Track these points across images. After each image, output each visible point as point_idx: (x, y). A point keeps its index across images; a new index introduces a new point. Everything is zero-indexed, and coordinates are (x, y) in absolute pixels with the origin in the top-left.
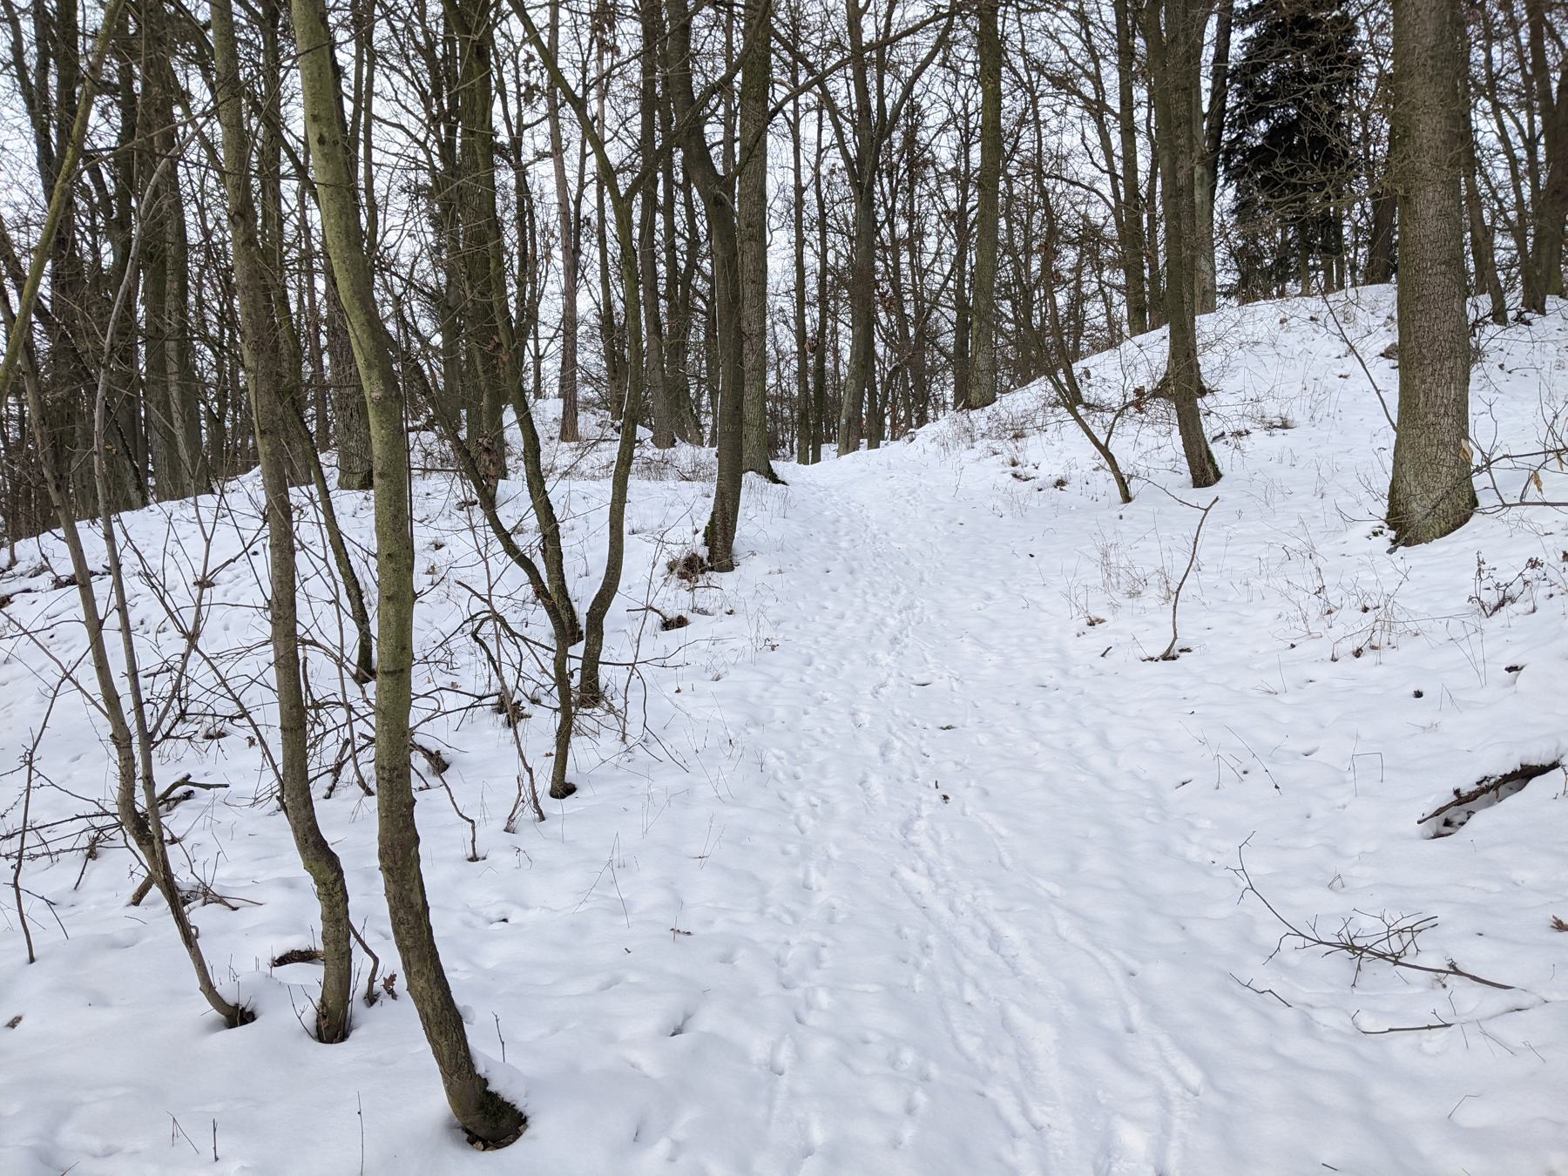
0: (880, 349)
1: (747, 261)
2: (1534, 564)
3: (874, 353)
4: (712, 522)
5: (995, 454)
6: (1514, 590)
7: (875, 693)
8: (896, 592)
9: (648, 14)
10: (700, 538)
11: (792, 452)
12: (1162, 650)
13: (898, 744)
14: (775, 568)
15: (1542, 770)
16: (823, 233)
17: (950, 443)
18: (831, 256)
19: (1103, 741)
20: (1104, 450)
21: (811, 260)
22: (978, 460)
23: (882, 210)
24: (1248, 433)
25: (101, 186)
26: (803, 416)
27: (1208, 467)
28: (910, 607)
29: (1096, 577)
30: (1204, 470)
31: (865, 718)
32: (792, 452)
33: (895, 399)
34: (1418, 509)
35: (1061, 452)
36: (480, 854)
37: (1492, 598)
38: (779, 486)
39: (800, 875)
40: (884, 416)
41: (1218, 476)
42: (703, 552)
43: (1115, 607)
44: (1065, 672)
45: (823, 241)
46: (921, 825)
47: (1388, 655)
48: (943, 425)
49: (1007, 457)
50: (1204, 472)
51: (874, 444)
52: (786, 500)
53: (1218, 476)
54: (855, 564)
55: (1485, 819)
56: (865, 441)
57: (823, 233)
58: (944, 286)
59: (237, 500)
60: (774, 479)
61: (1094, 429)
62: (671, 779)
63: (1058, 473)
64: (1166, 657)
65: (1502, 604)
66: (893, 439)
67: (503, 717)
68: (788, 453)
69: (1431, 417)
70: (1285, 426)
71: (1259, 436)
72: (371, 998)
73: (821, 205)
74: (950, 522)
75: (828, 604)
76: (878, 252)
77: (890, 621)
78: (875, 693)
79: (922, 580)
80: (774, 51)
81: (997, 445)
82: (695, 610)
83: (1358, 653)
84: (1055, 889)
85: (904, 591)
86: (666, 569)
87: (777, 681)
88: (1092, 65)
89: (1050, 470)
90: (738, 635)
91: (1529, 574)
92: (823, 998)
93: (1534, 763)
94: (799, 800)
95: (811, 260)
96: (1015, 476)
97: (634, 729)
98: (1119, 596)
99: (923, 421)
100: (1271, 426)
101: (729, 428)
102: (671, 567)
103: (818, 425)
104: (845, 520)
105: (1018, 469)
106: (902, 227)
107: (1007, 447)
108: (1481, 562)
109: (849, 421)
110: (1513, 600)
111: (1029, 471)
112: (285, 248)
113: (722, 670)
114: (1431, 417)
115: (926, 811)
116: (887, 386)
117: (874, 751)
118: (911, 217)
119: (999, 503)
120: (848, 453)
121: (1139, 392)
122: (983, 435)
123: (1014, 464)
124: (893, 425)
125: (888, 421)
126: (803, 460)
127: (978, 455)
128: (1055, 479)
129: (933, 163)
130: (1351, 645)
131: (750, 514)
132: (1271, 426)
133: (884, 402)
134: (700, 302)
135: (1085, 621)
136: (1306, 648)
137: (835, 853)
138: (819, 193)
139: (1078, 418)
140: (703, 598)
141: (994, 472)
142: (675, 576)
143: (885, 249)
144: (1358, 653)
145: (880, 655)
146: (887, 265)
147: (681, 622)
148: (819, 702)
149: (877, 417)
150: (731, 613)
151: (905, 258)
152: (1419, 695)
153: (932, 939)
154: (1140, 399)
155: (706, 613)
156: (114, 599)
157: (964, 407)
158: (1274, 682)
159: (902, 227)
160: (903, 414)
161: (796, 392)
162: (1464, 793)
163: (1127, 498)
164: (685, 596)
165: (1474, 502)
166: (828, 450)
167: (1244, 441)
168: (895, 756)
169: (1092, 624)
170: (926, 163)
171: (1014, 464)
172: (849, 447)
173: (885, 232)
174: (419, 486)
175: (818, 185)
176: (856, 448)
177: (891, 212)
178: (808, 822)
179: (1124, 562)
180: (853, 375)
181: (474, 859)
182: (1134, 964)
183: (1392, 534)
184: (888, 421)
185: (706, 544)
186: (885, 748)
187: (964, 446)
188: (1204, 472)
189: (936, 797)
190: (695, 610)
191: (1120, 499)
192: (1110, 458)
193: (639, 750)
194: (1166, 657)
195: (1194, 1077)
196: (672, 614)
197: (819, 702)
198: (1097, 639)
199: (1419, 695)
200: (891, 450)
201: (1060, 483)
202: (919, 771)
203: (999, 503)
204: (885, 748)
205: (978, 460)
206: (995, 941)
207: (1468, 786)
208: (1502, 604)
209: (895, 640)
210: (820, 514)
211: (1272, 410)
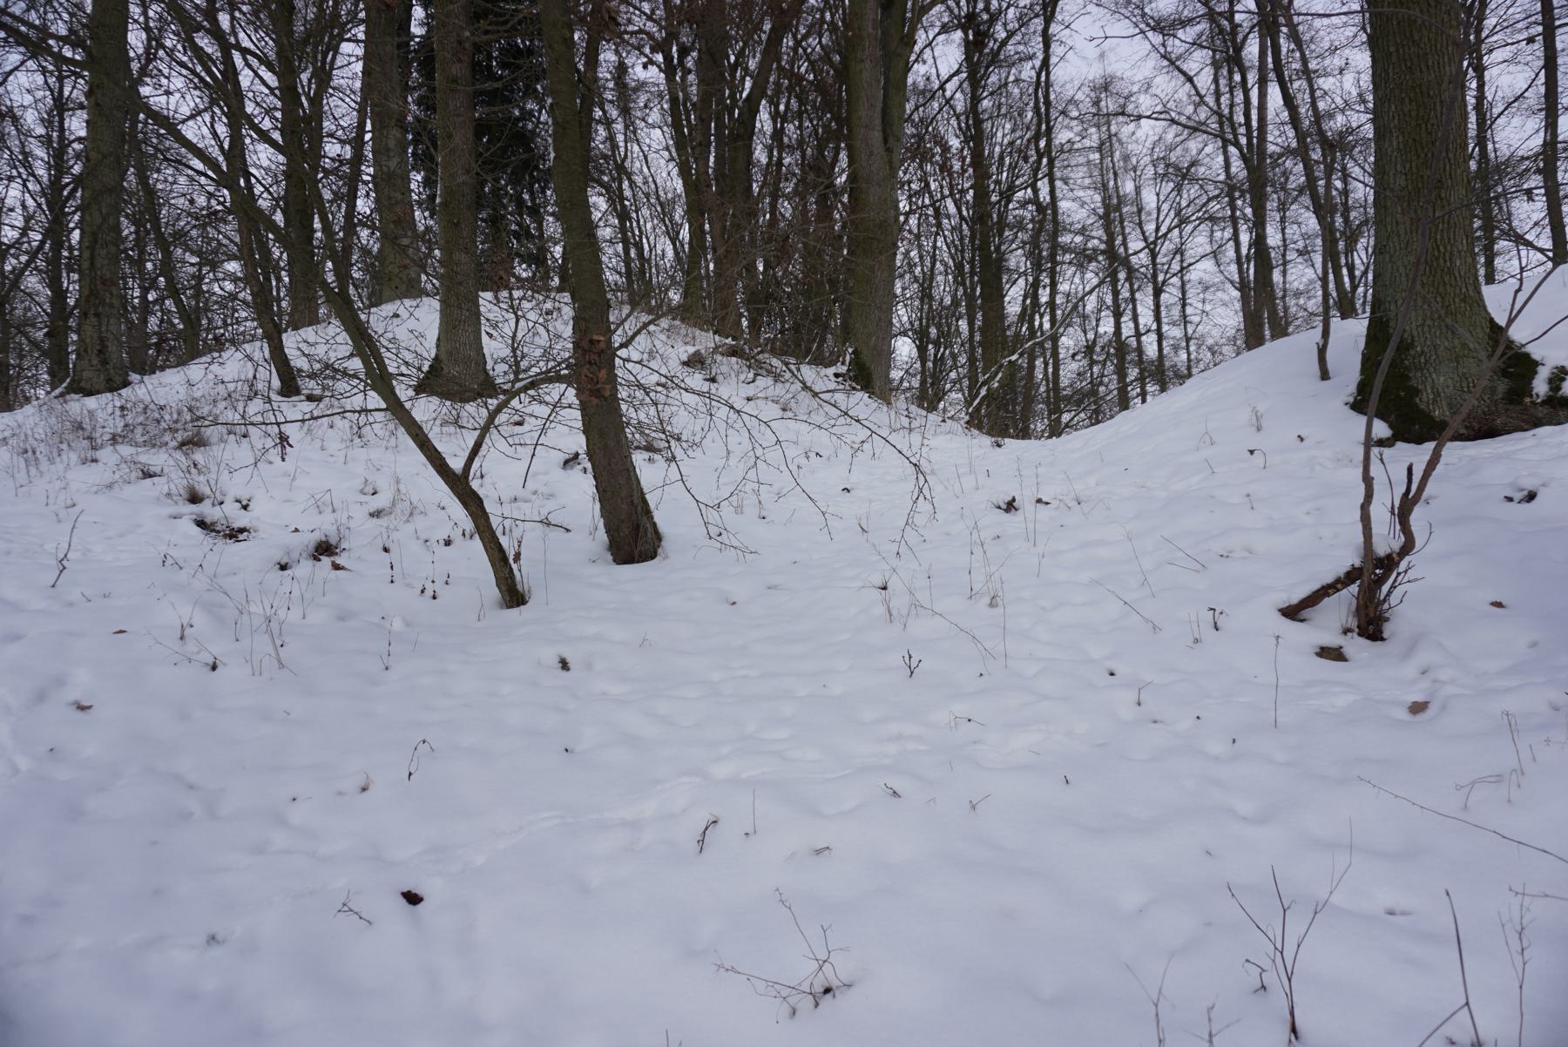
5: (147, 475)
9: (1480, 2)
17: (42, 448)
22: (110, 486)
25: (211, 179)
49: (177, 482)
59: (140, 45)
74: (40, 697)
80: (550, 136)
81: (155, 459)
96: (201, 524)
105: (207, 510)
112: (902, 218)
122: (114, 439)
127: (108, 477)
156: (1213, 87)
157: (70, 390)
171: (195, 498)
187: (74, 457)
191: (493, 592)
205: (110, 486)
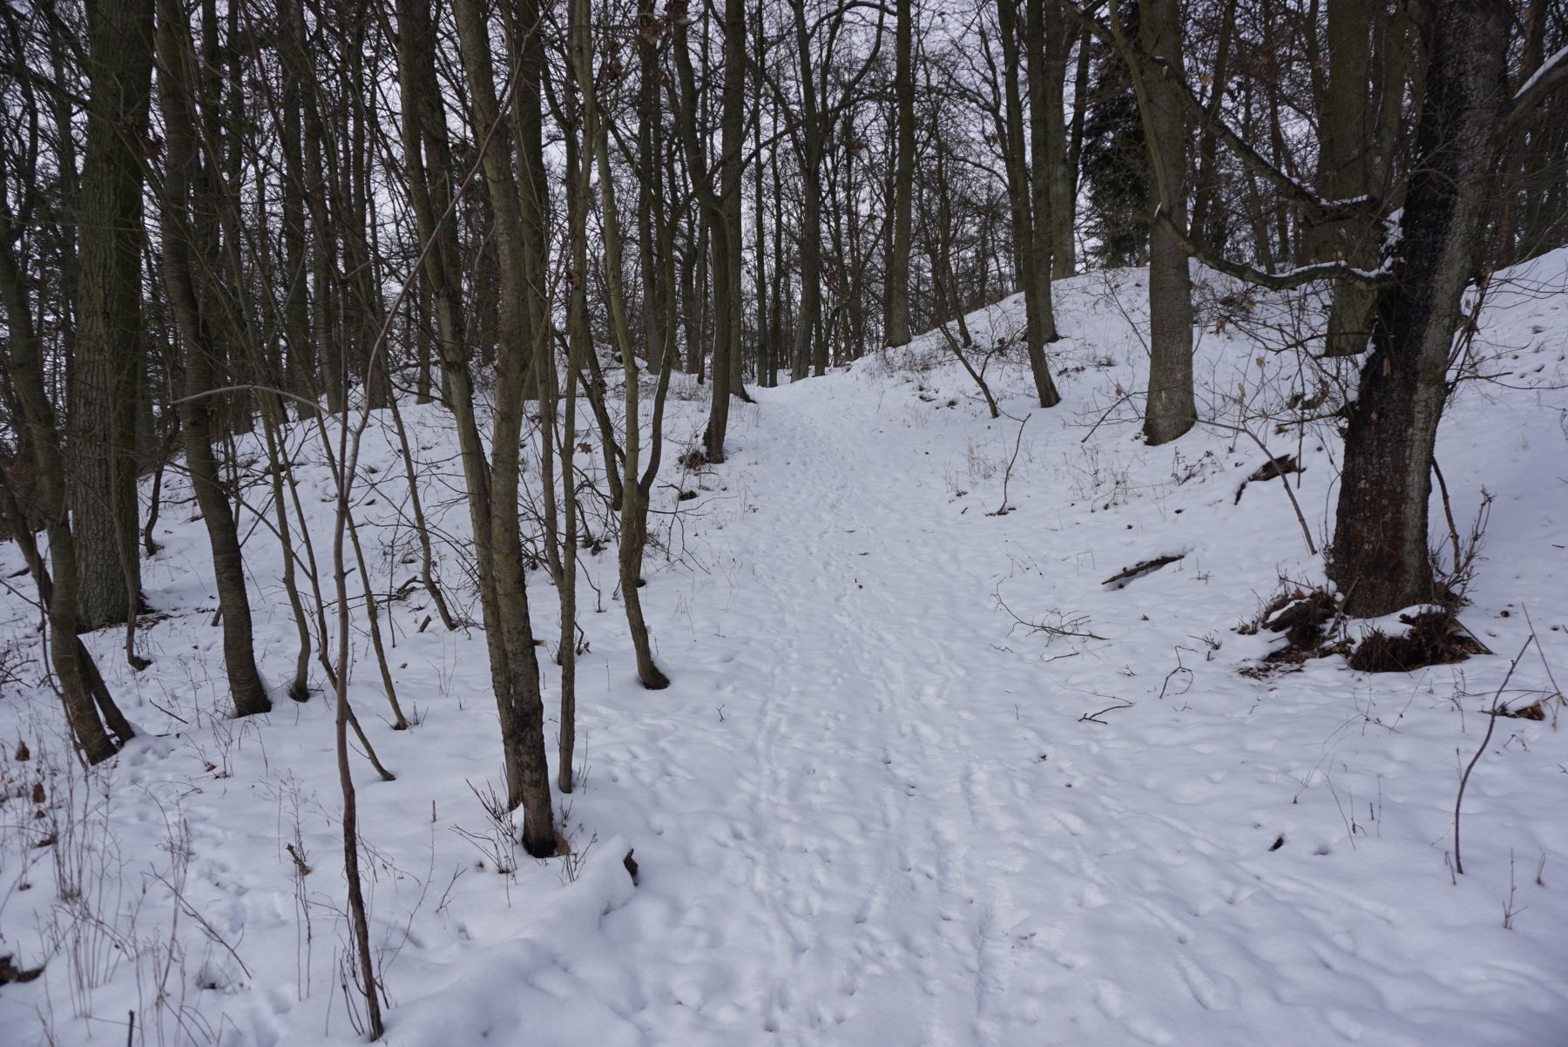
0: (824, 289)
1: (729, 233)
2: (1209, 454)
3: (821, 296)
4: (709, 429)
6: (1195, 470)
7: (821, 536)
8: (835, 477)
10: (700, 440)
11: (753, 376)
12: (998, 508)
13: (834, 563)
14: (753, 461)
15: (1173, 559)
16: (778, 200)
18: (784, 219)
19: (954, 557)
20: (980, 380)
21: (769, 222)
23: (826, 182)
24: (1083, 369)
26: (762, 347)
27: (1051, 393)
28: (844, 487)
29: (965, 466)
30: (1048, 396)
31: (814, 549)
32: (753, 376)
33: (837, 332)
34: (1163, 424)
35: (954, 380)
36: (602, 608)
37: (1183, 475)
38: (751, 404)
39: (780, 616)
40: (828, 346)
41: (1058, 400)
42: (703, 450)
43: (974, 484)
44: (939, 523)
45: (778, 206)
46: (845, 599)
47: (1121, 508)
48: (869, 360)
49: (916, 384)
50: (1049, 397)
51: (820, 372)
52: (758, 414)
53: (1058, 400)
54: (807, 459)
55: (1136, 583)
56: (812, 368)
57: (778, 200)
58: (876, 243)
60: (747, 399)
61: (974, 367)
62: (700, 577)
63: (951, 396)
64: (1001, 513)
65: (1188, 478)
66: (835, 366)
67: (590, 549)
68: (750, 376)
69: (1169, 365)
70: (1109, 364)
71: (1090, 371)
72: (579, 653)
73: (777, 178)
75: (790, 485)
76: (822, 216)
77: (831, 495)
78: (821, 536)
79: (852, 469)
81: (909, 375)
82: (701, 487)
83: (1106, 507)
84: (915, 620)
85: (840, 477)
86: (677, 462)
87: (759, 530)
88: (990, 72)
89: (946, 394)
90: (731, 506)
91: (1206, 460)
92: (795, 656)
93: (1169, 555)
94: (777, 588)
95: (769, 222)
96: (921, 398)
97: (676, 550)
98: (978, 478)
99: (859, 353)
100: (1100, 364)
101: (721, 364)
102: (681, 460)
103: (774, 355)
104: (799, 429)
105: (924, 393)
106: (841, 195)
107: (916, 377)
108: (1177, 453)
109: (800, 353)
110: (1194, 475)
111: (932, 394)
113: (723, 523)
114: (1169, 365)
115: (849, 592)
116: (831, 322)
117: (820, 566)
118: (848, 187)
119: (908, 418)
120: (799, 379)
121: (1001, 341)
123: (921, 389)
124: (837, 353)
125: (831, 351)
126: (763, 383)
128: (947, 401)
129: (867, 146)
130: (1102, 503)
131: (733, 424)
132: (1100, 364)
133: (829, 334)
134: (677, 253)
135: (954, 493)
136: (1080, 505)
137: (797, 609)
138: (775, 168)
139: (961, 358)
140: (708, 480)
141: (908, 395)
142: (682, 467)
143: (828, 213)
144: (1106, 507)
145: (824, 515)
146: (830, 226)
147: (692, 495)
148: (786, 541)
149: (822, 348)
150: (725, 489)
151: (844, 219)
152: (1130, 527)
153: (848, 638)
154: (1002, 348)
155: (708, 489)
158: (1056, 524)
159: (841, 195)
160: (843, 345)
161: (756, 327)
162: (1129, 568)
163: (995, 415)
164: (695, 480)
165: (1195, 416)
166: (783, 375)
167: (1081, 375)
168: (832, 569)
169: (959, 495)
170: (861, 147)
171: (921, 389)
172: (799, 374)
173: (828, 202)
174: (578, 401)
175: (774, 162)
176: (805, 375)
177: (832, 185)
178: (782, 597)
179: (982, 456)
180: (803, 316)
181: (600, 611)
182: (946, 643)
183: (1146, 438)
184: (831, 351)
185: (705, 444)
186: (826, 565)
188: (1049, 397)
189: (856, 586)
190: (701, 487)
192: (983, 386)
193: (679, 565)
194: (1001, 513)
195: (961, 673)
196: (686, 489)
197: (786, 541)
198: (961, 503)
199: (1130, 527)
200: (834, 376)
201: (952, 404)
202: (846, 575)
203: (908, 418)
204: (826, 565)
206: (880, 639)
207: (1131, 566)
208: (1188, 478)
209: (833, 506)
210: (781, 424)
211: (1102, 353)
